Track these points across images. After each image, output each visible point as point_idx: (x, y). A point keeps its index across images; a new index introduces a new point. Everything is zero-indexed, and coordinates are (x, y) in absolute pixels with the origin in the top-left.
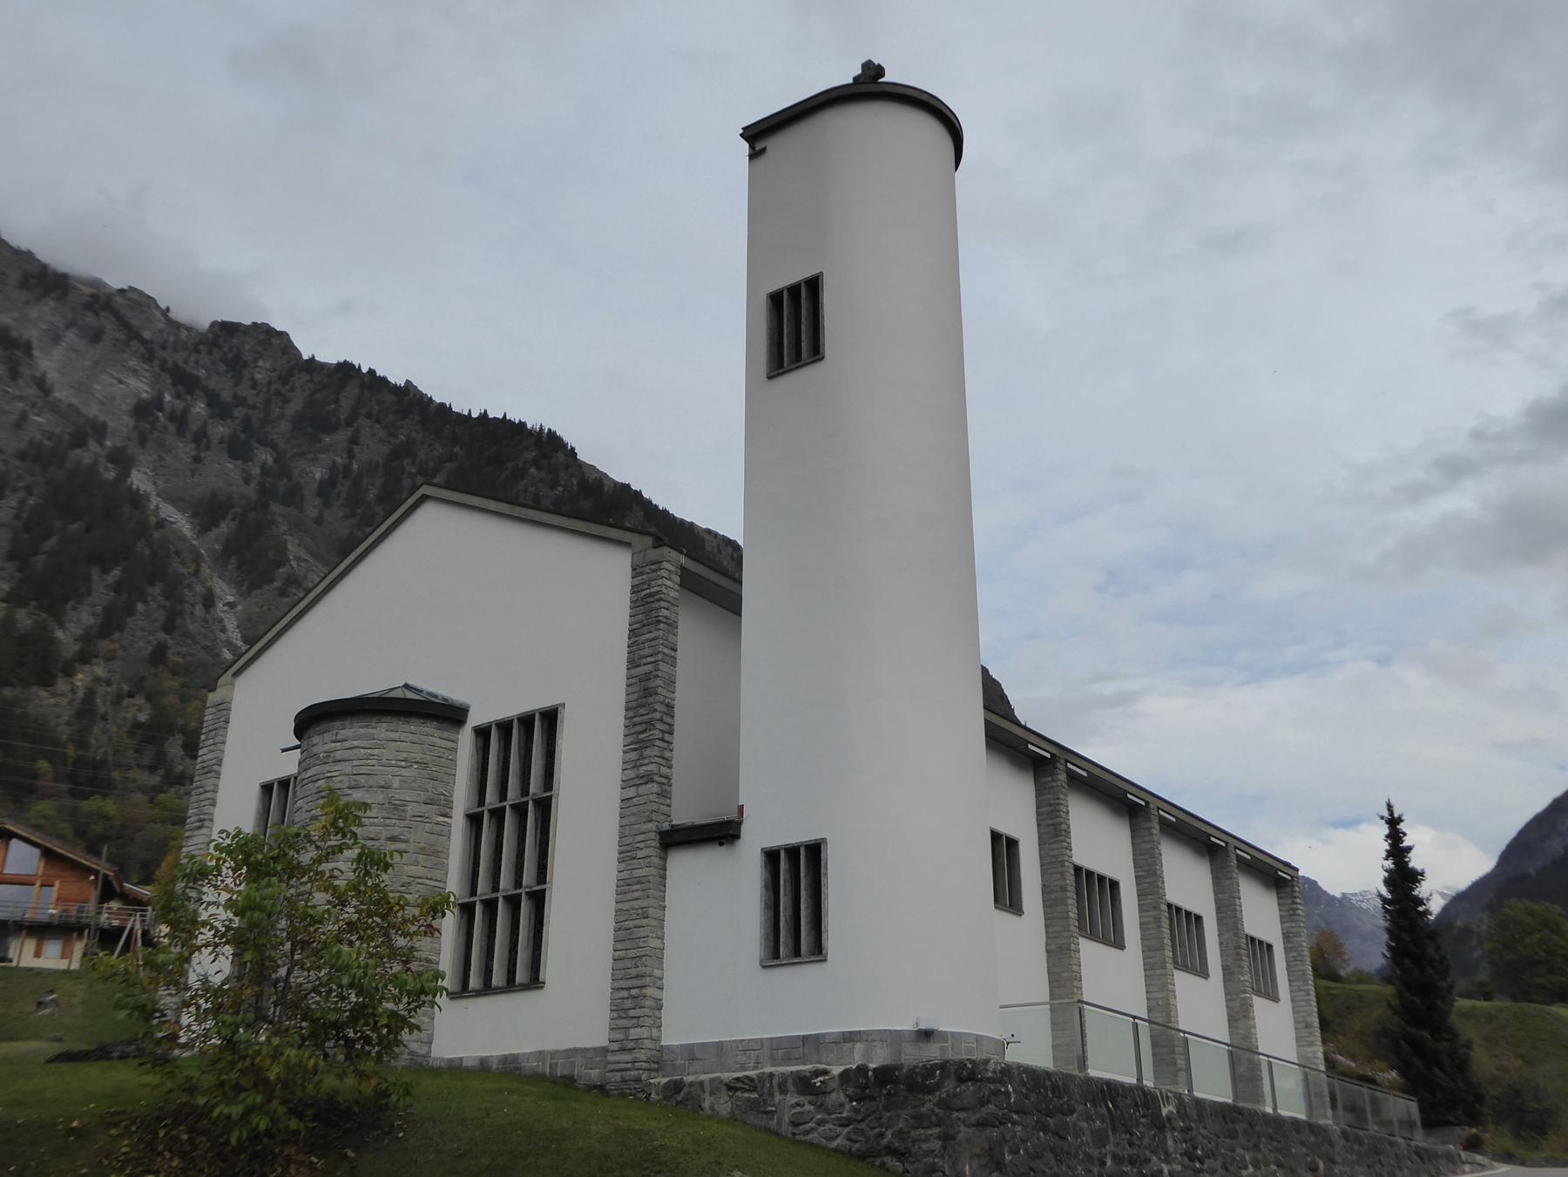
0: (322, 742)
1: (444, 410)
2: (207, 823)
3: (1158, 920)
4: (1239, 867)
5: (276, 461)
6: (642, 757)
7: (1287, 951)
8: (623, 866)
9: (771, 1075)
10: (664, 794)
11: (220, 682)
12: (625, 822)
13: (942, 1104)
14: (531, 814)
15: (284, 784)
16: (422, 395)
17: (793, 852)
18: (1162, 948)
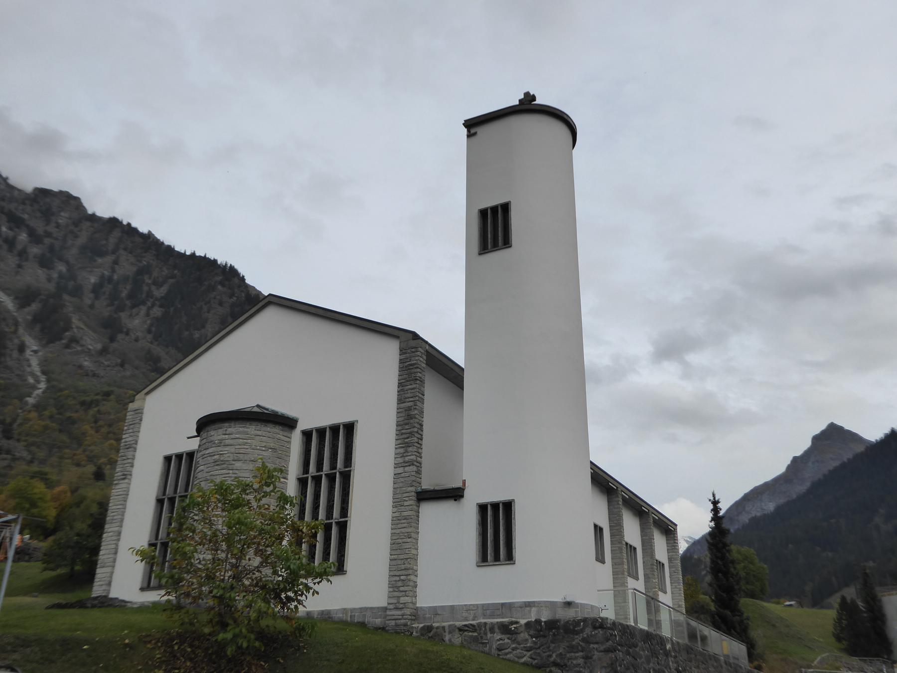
0: (216, 434)
1: (170, 250)
2: (129, 477)
3: (621, 549)
4: (655, 526)
5: (68, 270)
6: (406, 451)
7: (670, 567)
8: (395, 509)
9: (485, 623)
10: (419, 472)
11: (137, 397)
12: (396, 486)
13: (583, 640)
14: (338, 480)
15: (191, 455)
16: (158, 240)
17: (495, 506)
18: (622, 563)
